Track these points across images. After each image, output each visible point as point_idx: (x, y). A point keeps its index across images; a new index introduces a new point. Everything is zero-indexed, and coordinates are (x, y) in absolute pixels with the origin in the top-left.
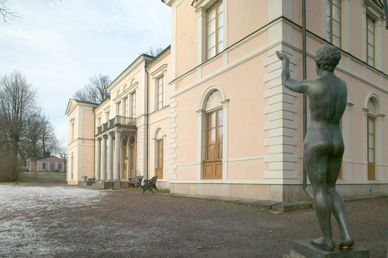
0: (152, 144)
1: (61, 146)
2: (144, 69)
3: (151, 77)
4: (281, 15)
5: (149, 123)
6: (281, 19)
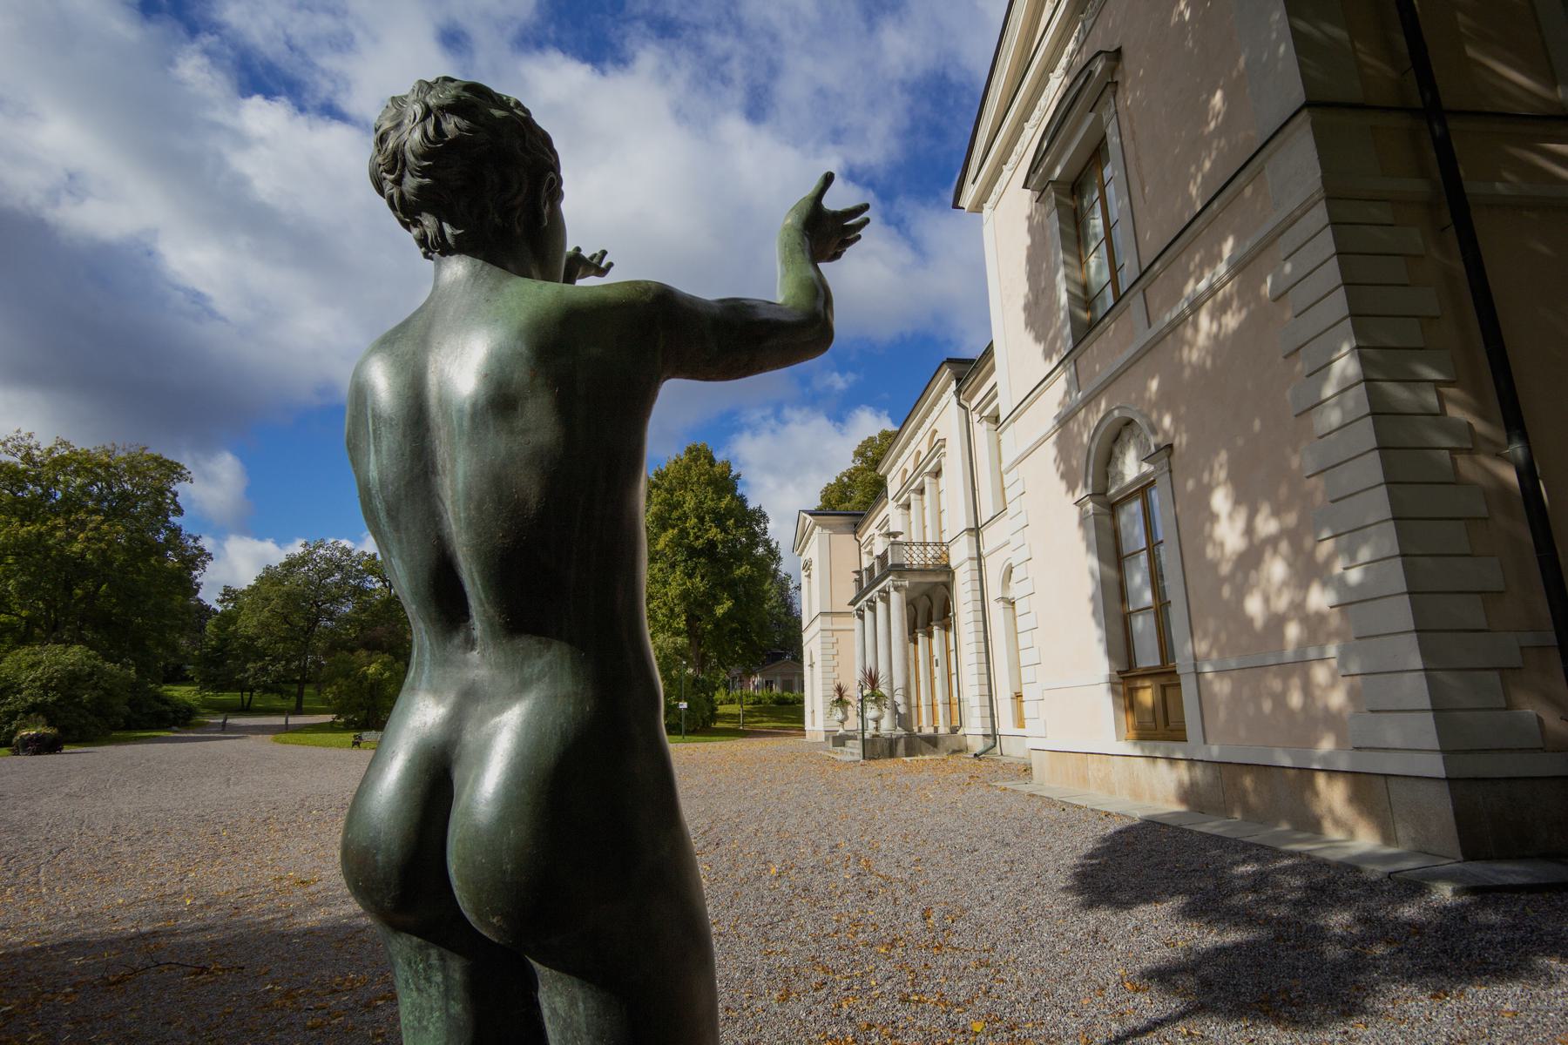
0: (996, 612)
1: (548, 657)
2: (954, 399)
3: (975, 417)
4: (1302, 100)
5: (984, 552)
6: (1305, 113)
